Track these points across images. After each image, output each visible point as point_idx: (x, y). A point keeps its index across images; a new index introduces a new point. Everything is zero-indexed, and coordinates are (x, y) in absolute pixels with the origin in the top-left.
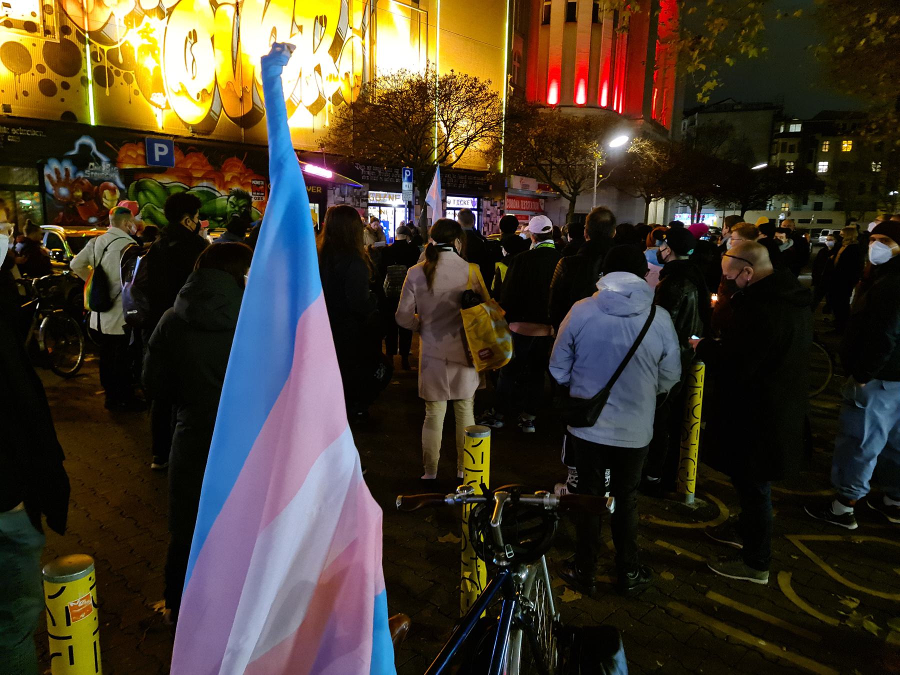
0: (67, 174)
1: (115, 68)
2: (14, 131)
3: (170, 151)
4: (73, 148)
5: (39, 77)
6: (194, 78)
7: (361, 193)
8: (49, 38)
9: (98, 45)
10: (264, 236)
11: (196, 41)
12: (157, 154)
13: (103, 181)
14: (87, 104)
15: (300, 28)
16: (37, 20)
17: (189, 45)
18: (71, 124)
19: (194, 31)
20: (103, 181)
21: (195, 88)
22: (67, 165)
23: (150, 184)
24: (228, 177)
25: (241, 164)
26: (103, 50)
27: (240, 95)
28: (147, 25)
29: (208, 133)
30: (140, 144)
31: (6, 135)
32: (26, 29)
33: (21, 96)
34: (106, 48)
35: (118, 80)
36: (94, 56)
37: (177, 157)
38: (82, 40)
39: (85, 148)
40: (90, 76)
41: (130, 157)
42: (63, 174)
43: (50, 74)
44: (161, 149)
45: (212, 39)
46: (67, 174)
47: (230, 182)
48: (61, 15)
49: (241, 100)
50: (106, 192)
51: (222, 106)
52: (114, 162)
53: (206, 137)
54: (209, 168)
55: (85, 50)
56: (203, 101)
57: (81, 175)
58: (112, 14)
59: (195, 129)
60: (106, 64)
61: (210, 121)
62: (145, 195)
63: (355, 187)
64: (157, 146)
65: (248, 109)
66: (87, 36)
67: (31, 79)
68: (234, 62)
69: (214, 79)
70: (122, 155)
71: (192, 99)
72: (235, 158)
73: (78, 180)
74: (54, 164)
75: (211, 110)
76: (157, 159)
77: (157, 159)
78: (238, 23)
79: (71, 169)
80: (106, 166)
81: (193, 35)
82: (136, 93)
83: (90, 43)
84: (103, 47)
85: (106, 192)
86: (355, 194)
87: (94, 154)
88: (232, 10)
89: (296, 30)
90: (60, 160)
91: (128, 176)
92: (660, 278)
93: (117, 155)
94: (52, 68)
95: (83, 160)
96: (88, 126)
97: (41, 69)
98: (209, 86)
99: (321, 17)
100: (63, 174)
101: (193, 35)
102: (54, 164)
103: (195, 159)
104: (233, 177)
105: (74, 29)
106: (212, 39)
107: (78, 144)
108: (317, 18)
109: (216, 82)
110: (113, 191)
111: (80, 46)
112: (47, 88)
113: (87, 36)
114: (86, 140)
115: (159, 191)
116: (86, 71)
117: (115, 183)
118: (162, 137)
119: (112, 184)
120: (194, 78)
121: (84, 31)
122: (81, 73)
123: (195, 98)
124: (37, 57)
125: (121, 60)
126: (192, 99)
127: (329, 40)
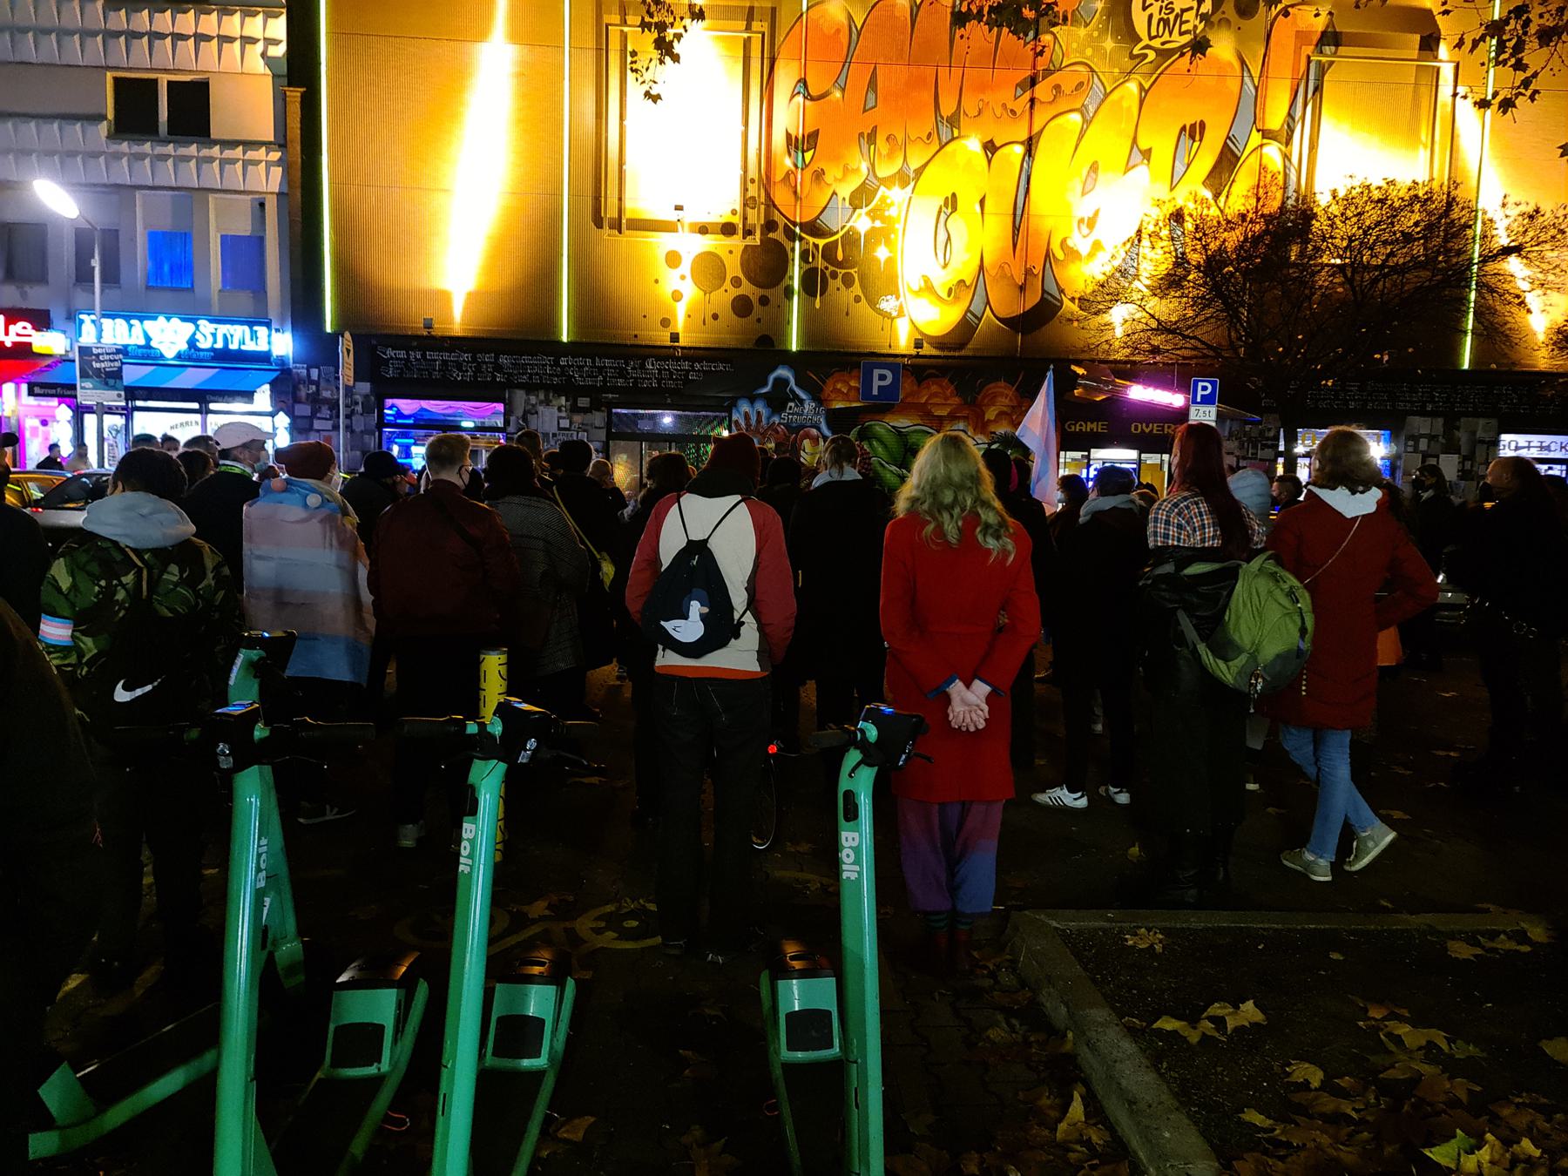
0: (759, 420)
1: (831, 268)
2: (697, 366)
3: (896, 379)
4: (765, 384)
5: (735, 292)
6: (945, 266)
7: (1261, 433)
8: (749, 241)
9: (812, 240)
10: (446, 1135)
11: (954, 209)
12: (876, 383)
13: (804, 427)
14: (789, 322)
15: (1147, 154)
16: (737, 220)
17: (943, 216)
18: (767, 349)
19: (954, 195)
20: (804, 427)
21: (943, 280)
22: (760, 406)
23: (879, 429)
24: (991, 414)
25: (1010, 392)
26: (816, 246)
27: (1020, 280)
28: (883, 199)
29: (962, 346)
30: (854, 373)
31: (688, 371)
32: (723, 233)
33: (709, 319)
34: (821, 242)
35: (834, 284)
36: (804, 255)
37: (907, 385)
38: (791, 236)
39: (781, 383)
40: (796, 284)
41: (839, 391)
42: (754, 419)
43: (747, 288)
44: (882, 377)
45: (982, 202)
46: (759, 420)
47: (995, 421)
48: (767, 206)
49: (1022, 288)
50: (806, 442)
51: (988, 302)
52: (819, 400)
53: (963, 353)
54: (956, 400)
55: (793, 250)
56: (957, 299)
57: (776, 419)
58: (834, 193)
59: (939, 343)
60: (820, 263)
61: (966, 327)
62: (871, 445)
63: (1246, 422)
64: (876, 372)
65: (1033, 299)
66: (797, 230)
67: (724, 297)
68: (1016, 229)
69: (978, 262)
70: (828, 389)
71: (939, 298)
72: (1002, 383)
73: (772, 427)
74: (744, 407)
75: (968, 310)
76: (875, 392)
77: (875, 392)
78: (1030, 168)
79: (764, 412)
80: (809, 406)
81: (952, 202)
82: (857, 299)
83: (801, 239)
84: (817, 241)
85: (806, 442)
86: (1245, 434)
87: (792, 391)
88: (1019, 150)
89: (1137, 157)
90: (752, 401)
91: (839, 420)
92: (155, 318)
93: (822, 390)
94: (750, 279)
95: (778, 400)
96: (788, 352)
97: (736, 282)
98: (968, 272)
99: (1193, 126)
100: (754, 419)
101: (952, 202)
102: (744, 407)
103: (934, 388)
104: (1001, 414)
105: (781, 221)
106: (982, 202)
107: (771, 378)
108: (1183, 128)
109: (981, 267)
110: (815, 441)
111: (787, 245)
112: (741, 306)
113: (797, 230)
114: (783, 372)
115: (890, 440)
116: (792, 278)
117: (819, 429)
118: (890, 361)
119: (814, 431)
120: (945, 266)
121: (795, 224)
122: (786, 282)
123: (944, 295)
124: (734, 268)
125: (840, 256)
126: (939, 298)
127: (1205, 161)
